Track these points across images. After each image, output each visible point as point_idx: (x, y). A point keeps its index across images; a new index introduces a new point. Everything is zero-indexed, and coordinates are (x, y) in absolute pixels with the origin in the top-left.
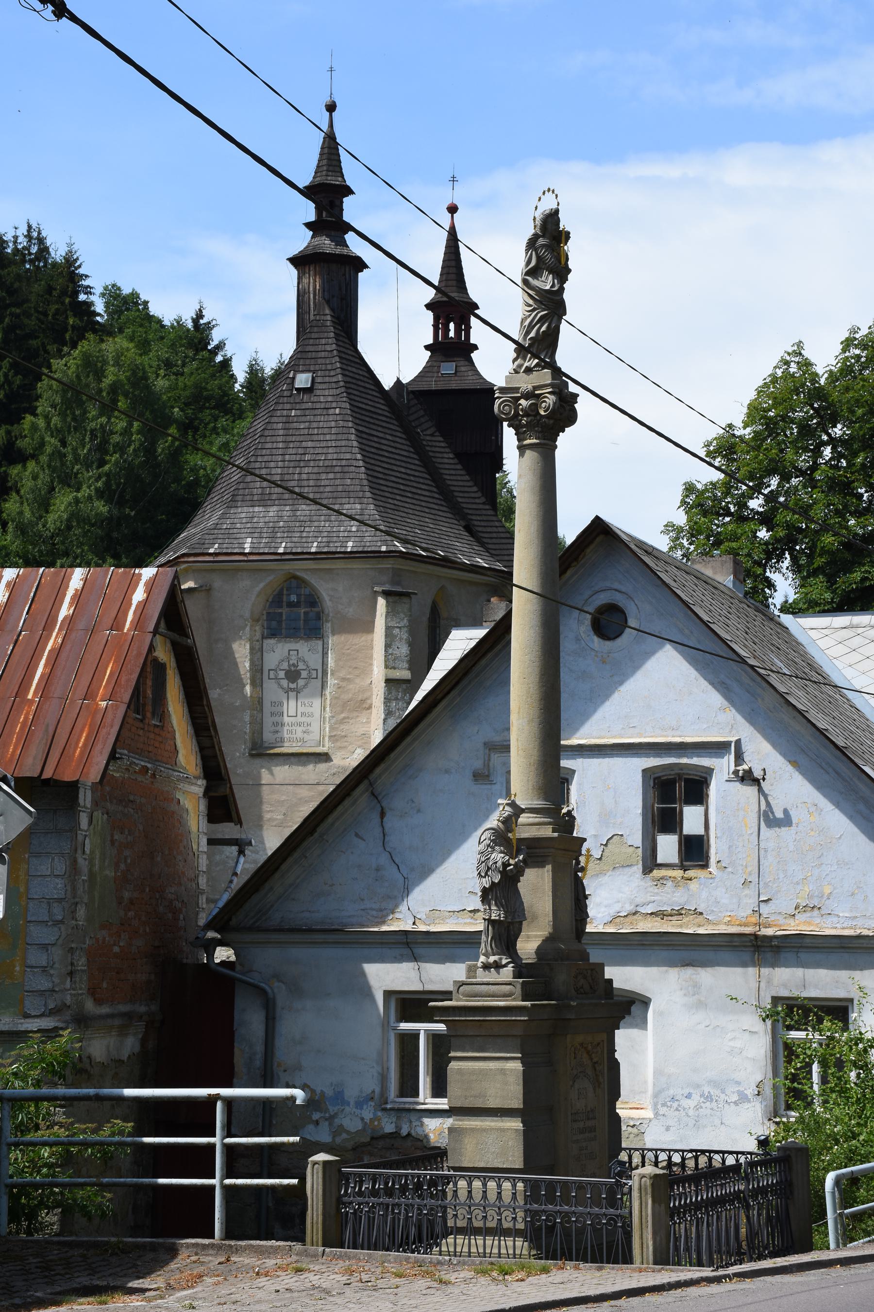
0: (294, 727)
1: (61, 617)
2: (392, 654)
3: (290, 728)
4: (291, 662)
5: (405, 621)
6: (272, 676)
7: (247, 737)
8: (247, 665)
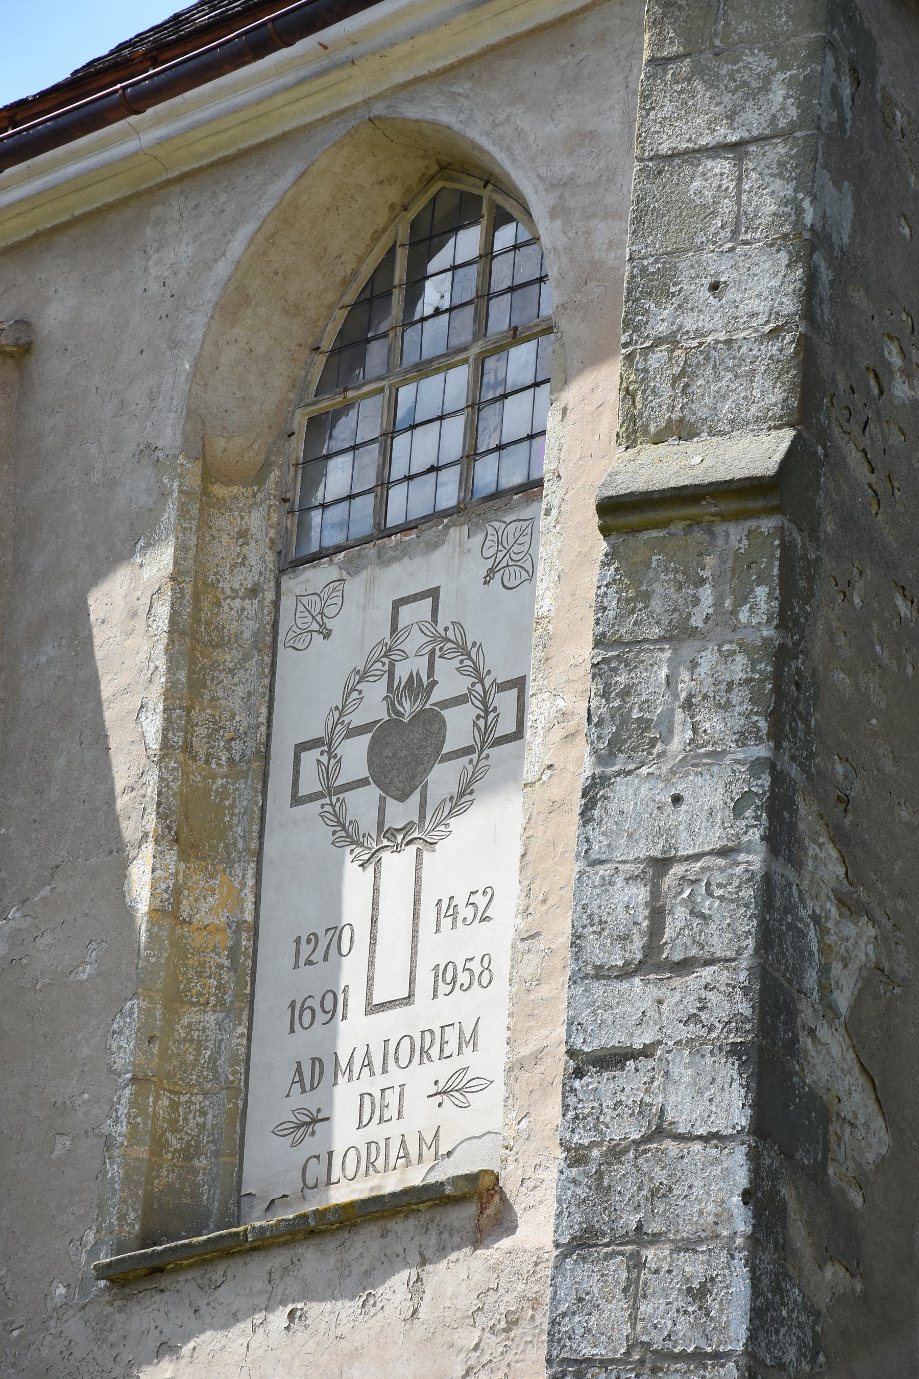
0: (396, 1076)
1: (143, 907)
2: (671, 341)
3: (373, 1084)
4: (402, 672)
5: (778, 94)
6: (310, 783)
7: (115, 1170)
8: (153, 725)
